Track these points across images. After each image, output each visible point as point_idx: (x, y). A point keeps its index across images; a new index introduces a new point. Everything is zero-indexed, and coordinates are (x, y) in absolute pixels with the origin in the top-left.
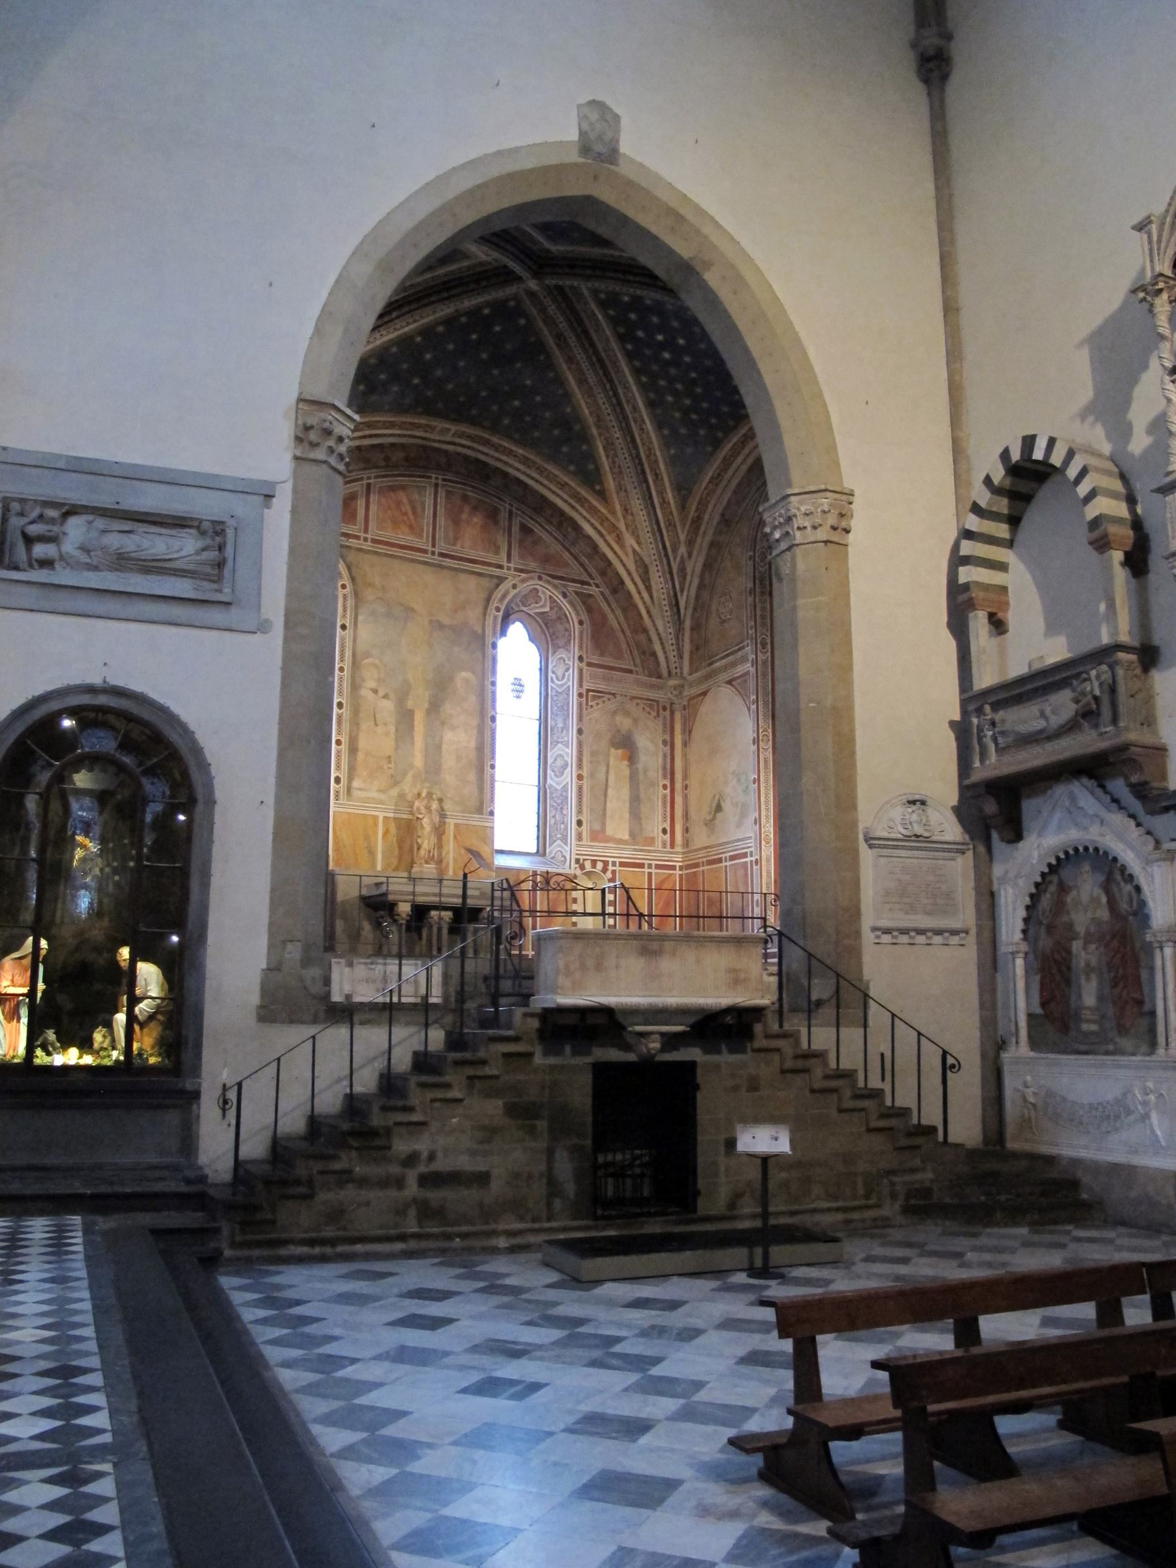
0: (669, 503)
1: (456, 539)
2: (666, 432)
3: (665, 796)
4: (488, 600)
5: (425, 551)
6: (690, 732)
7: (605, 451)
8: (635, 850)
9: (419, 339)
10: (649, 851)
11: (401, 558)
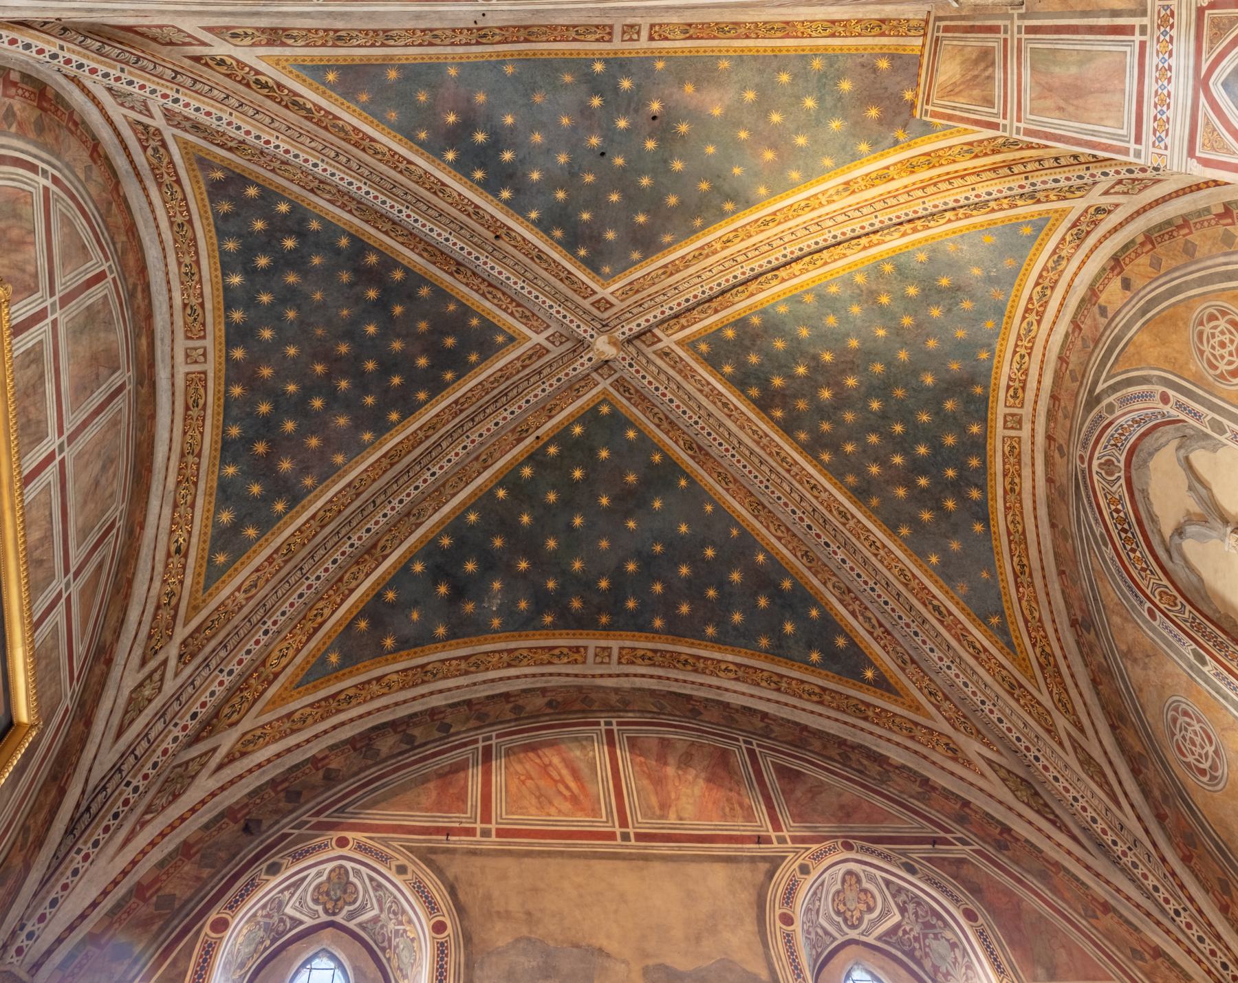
0: (986, 650)
1: (664, 806)
2: (904, 531)
4: (761, 905)
5: (611, 836)
9: (501, 493)
11: (561, 854)
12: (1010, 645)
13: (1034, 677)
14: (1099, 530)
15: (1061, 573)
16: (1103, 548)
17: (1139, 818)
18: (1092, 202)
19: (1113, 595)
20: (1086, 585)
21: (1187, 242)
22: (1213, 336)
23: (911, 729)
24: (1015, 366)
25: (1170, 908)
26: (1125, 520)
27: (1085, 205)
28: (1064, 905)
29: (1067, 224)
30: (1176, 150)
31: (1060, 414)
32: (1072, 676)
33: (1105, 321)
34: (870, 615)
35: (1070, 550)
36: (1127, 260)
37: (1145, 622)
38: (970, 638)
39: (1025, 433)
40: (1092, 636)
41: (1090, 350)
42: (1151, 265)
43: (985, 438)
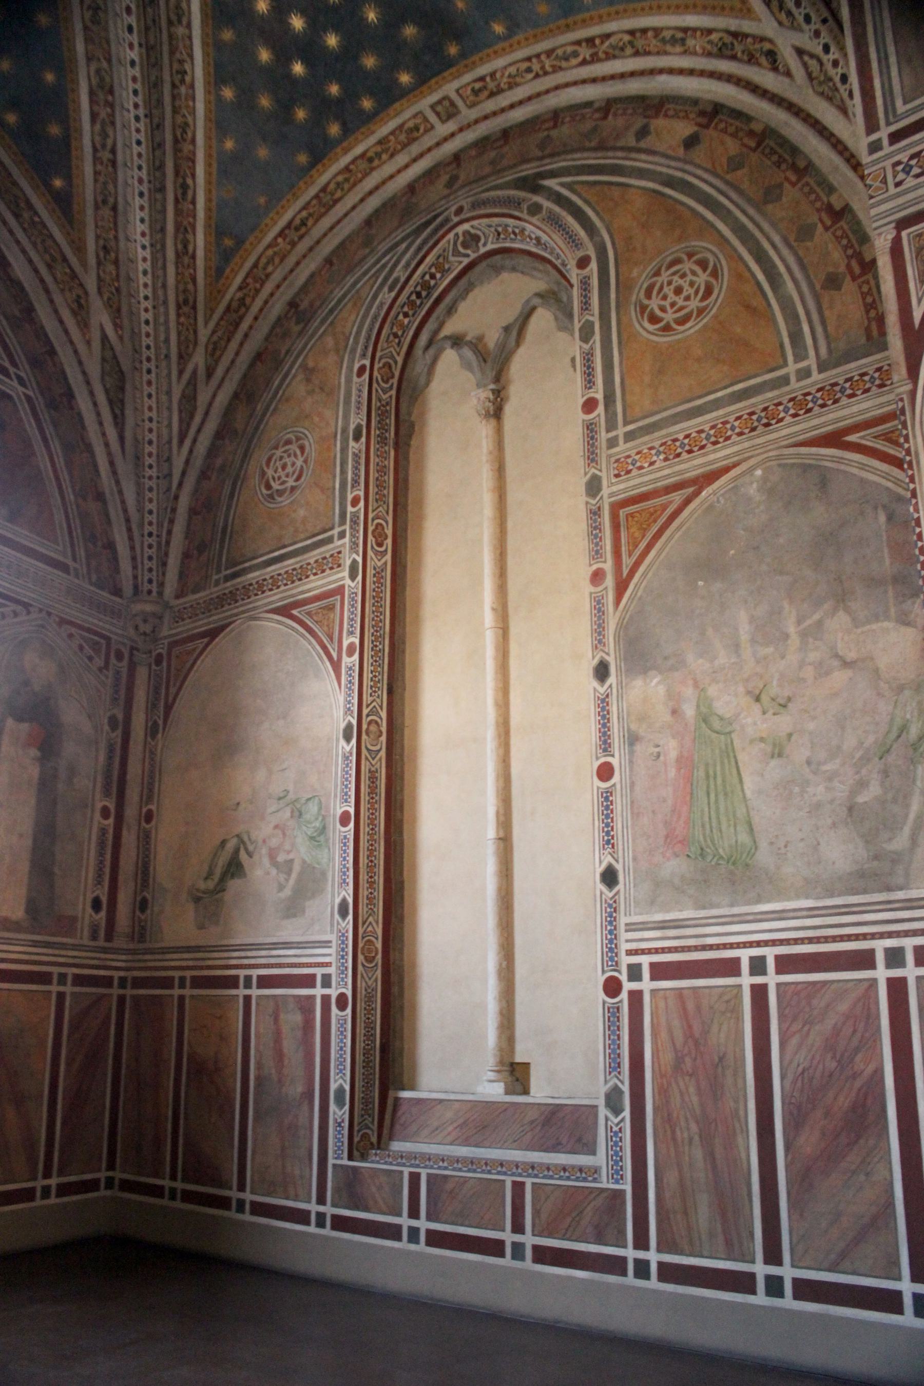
0: (193, 257)
2: (228, 93)
3: (103, 831)
6: (168, 708)
7: (92, 101)
8: (35, 944)
10: (63, 946)
12: (220, 272)
13: (213, 311)
14: (400, 273)
15: (328, 261)
16: (386, 289)
17: (187, 462)
18: (779, 42)
19: (349, 324)
20: (338, 293)
21: (780, 186)
22: (683, 276)
23: (55, 259)
24: (512, 70)
25: (147, 528)
26: (429, 289)
27: (769, 33)
28: (67, 477)
29: (733, 24)
30: (900, 200)
31: (493, 154)
32: (246, 335)
33: (631, 141)
34: (111, 133)
36: (722, 125)
37: (350, 368)
38: (190, 237)
39: (443, 129)
40: (296, 329)
41: (587, 144)
42: (730, 160)
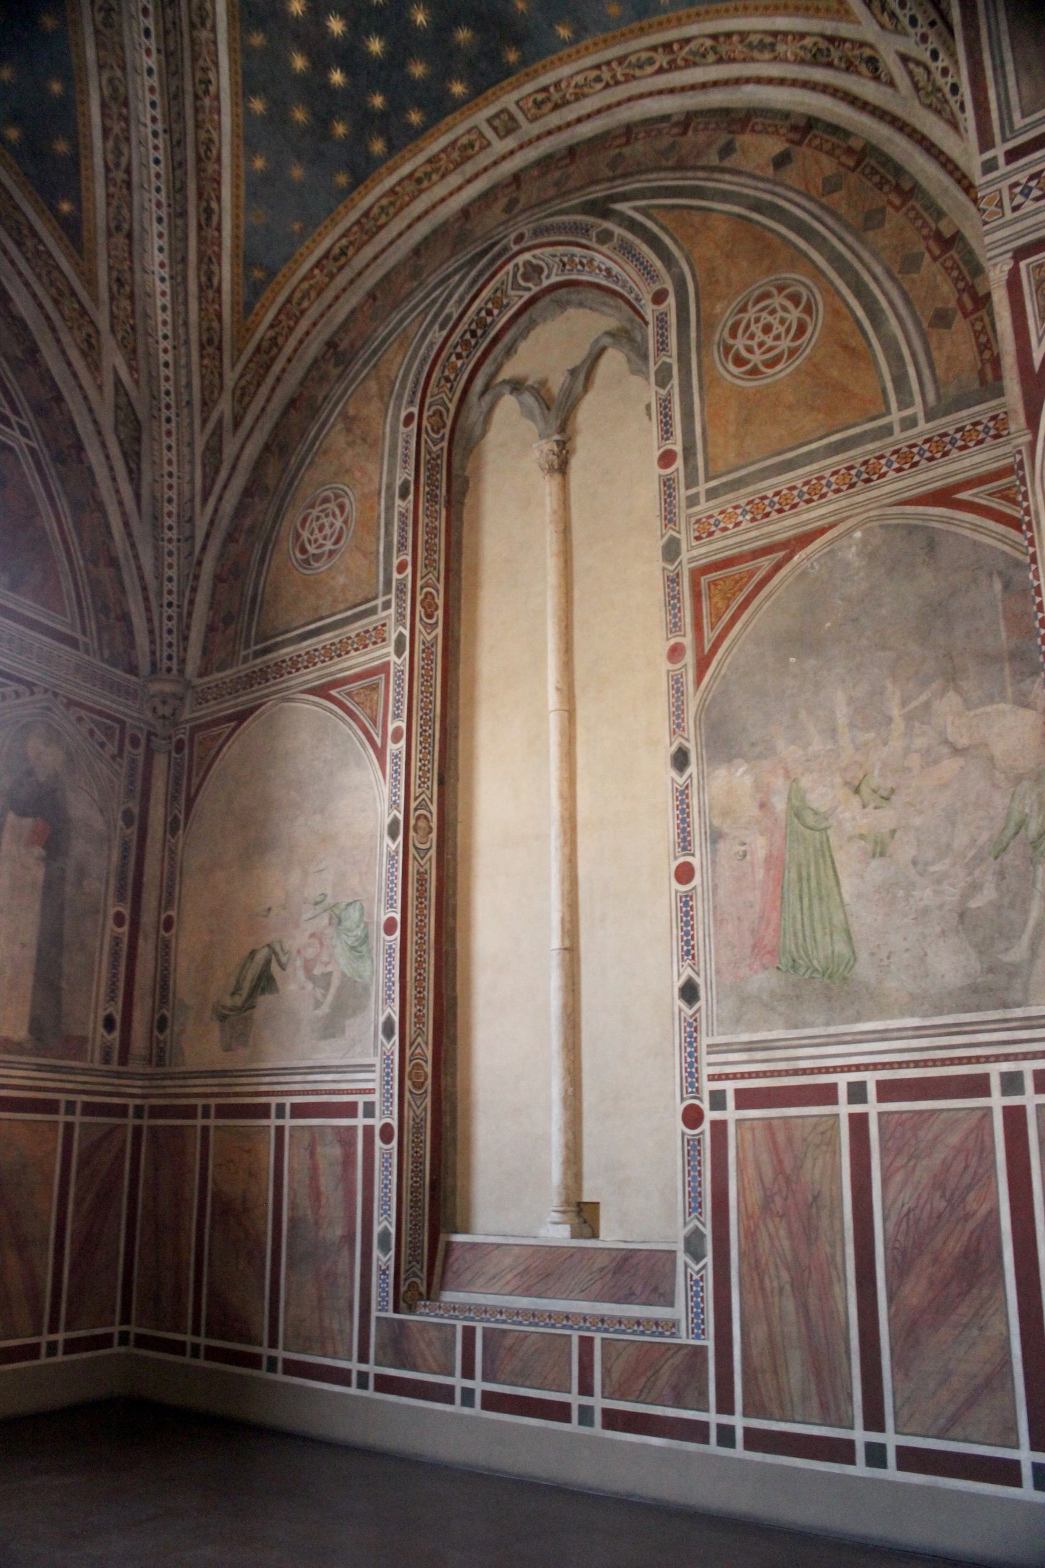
0: (219, 291)
2: (258, 105)
3: (117, 940)
6: (190, 801)
7: (105, 115)
8: (40, 1068)
10: (72, 1071)
12: (248, 307)
13: (240, 351)
14: (452, 309)
15: (372, 296)
16: (436, 327)
17: (212, 522)
18: (881, 47)
20: (382, 332)
21: (882, 210)
22: (773, 312)
24: (579, 79)
25: (167, 598)
26: (486, 327)
28: (76, 540)
29: (829, 27)
30: (1018, 227)
31: (557, 174)
32: (278, 379)
33: (714, 160)
34: (125, 151)
35: (404, 292)
36: (817, 142)
37: (396, 417)
38: (215, 268)
39: (501, 146)
40: (335, 372)
41: (664, 163)
42: (826, 180)
43: (455, 109)
